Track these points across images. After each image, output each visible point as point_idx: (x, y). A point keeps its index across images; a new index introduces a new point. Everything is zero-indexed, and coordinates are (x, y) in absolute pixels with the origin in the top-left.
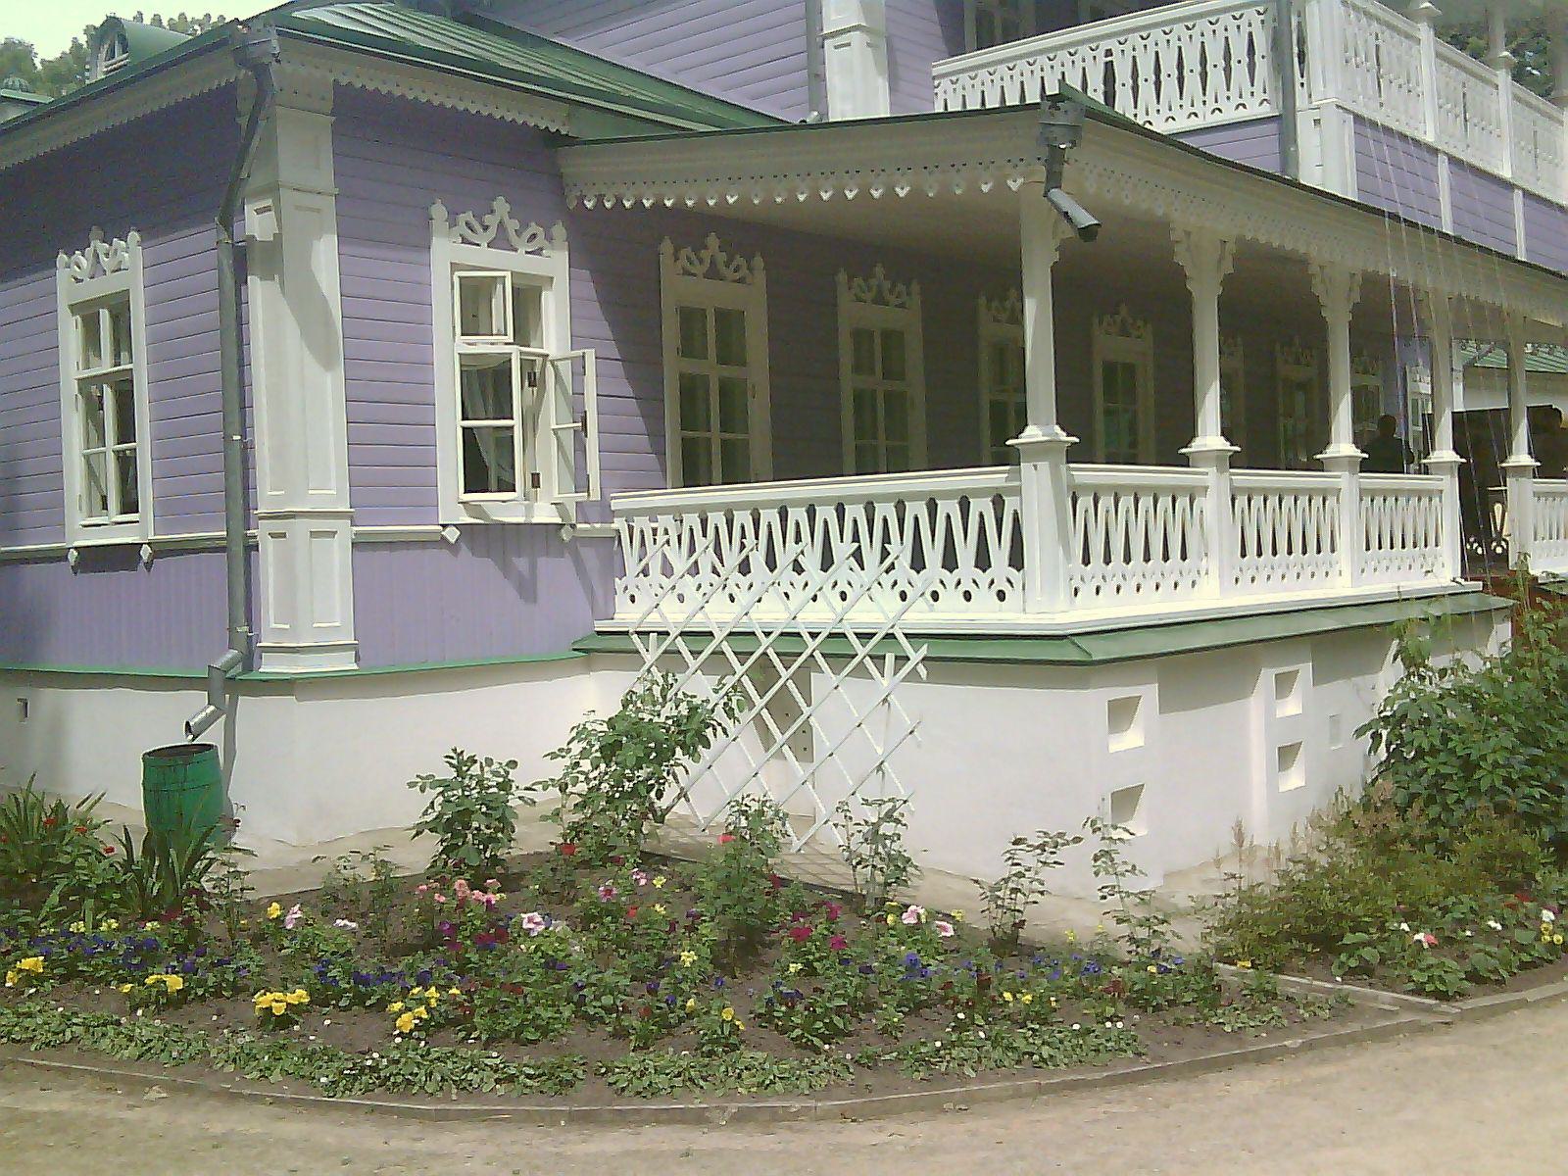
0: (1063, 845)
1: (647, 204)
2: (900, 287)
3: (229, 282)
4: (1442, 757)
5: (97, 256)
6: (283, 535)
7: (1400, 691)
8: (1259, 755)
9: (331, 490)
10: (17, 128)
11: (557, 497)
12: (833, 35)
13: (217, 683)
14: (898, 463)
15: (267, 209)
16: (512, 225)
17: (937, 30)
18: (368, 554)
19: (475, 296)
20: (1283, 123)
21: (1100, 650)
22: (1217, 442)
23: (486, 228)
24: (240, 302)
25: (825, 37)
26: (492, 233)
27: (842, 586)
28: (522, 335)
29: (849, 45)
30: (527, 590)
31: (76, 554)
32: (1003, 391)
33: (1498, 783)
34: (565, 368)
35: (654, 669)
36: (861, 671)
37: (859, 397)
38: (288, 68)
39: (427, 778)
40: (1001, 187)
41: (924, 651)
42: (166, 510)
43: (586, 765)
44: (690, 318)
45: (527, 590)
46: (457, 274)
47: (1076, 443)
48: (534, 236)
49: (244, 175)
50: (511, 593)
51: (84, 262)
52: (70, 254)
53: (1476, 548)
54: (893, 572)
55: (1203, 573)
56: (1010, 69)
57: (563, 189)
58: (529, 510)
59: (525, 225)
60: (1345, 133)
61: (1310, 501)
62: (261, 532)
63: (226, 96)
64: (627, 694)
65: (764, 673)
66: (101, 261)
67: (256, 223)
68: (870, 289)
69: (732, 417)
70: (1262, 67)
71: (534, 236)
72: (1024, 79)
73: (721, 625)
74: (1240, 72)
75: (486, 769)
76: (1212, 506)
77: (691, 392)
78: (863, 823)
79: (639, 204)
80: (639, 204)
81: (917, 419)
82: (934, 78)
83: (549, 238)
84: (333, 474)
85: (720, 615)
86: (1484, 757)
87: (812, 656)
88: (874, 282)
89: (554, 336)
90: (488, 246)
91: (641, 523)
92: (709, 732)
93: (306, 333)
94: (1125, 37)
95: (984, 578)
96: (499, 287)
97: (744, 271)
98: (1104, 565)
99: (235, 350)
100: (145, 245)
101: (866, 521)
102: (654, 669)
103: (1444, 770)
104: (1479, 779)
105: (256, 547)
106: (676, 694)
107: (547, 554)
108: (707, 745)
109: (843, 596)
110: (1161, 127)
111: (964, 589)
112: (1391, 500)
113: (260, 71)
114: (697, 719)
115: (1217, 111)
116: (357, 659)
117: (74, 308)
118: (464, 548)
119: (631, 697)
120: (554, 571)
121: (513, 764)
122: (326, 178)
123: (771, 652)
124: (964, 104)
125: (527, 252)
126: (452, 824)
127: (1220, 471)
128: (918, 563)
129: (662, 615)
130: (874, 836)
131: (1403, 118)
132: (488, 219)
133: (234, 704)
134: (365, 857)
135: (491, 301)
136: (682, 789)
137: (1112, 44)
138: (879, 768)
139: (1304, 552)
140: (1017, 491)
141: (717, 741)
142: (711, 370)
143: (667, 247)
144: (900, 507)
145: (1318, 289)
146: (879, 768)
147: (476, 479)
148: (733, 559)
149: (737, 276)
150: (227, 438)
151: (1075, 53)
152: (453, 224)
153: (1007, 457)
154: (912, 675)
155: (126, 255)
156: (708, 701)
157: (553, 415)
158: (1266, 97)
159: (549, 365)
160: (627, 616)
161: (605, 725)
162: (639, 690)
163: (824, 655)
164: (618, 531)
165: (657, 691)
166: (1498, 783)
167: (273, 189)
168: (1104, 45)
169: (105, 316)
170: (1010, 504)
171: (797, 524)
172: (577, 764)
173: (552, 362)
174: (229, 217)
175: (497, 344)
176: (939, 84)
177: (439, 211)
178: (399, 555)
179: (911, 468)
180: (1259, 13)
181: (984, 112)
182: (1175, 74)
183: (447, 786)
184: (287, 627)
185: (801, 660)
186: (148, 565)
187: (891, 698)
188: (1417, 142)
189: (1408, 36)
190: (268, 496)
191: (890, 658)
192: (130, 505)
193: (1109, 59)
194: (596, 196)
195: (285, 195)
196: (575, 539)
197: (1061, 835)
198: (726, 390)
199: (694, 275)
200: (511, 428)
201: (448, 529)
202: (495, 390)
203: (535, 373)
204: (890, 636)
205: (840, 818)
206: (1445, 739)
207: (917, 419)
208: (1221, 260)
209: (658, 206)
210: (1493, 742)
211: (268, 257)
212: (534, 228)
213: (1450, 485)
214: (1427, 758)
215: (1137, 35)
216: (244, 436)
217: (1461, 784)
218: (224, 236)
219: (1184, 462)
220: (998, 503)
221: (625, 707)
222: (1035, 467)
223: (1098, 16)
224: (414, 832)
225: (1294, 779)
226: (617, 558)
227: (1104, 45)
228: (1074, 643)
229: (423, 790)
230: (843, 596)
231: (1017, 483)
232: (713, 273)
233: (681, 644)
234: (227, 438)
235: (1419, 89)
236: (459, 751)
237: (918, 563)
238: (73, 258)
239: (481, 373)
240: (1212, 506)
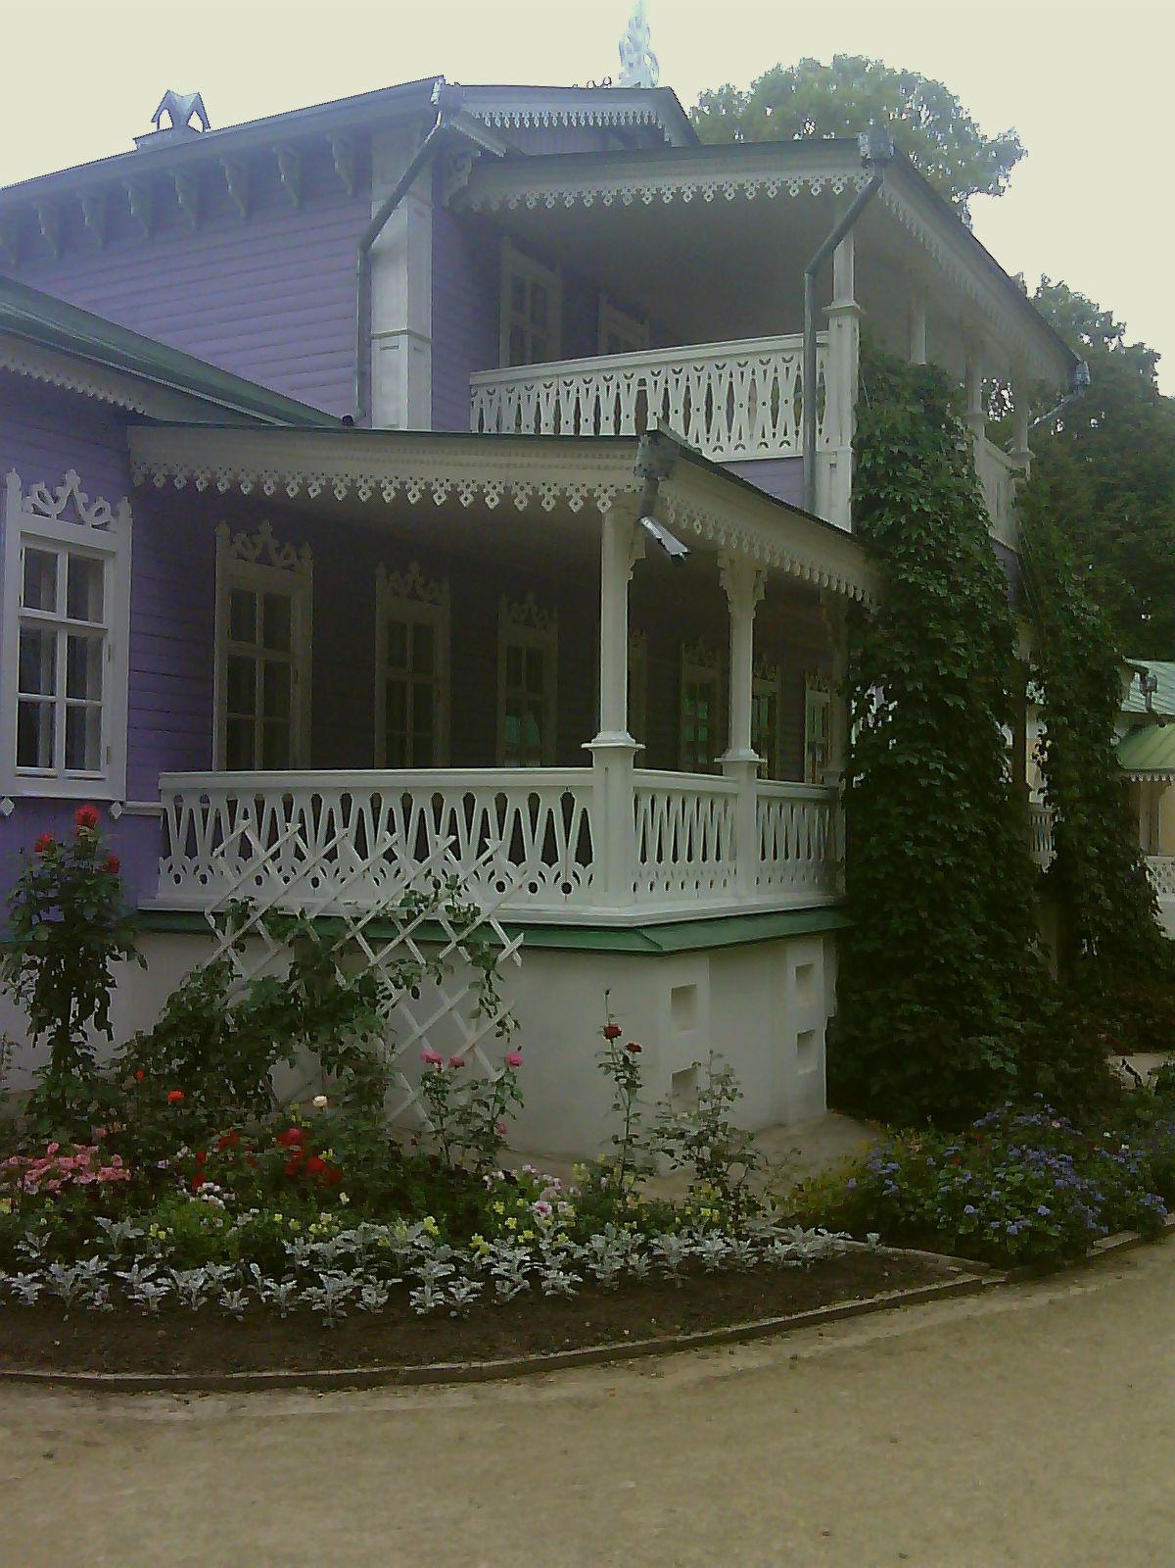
12: (381, 336)
16: (81, 498)
21: (668, 941)
22: (624, 739)
41: (520, 939)
47: (642, 749)
48: (100, 511)
61: (781, 809)
70: (786, 413)
71: (100, 511)
74: (764, 414)
83: (115, 514)
87: (403, 942)
95: (550, 872)
101: (528, 813)
123: (360, 939)
125: (93, 526)
128: (517, 855)
132: (60, 491)
139: (660, 860)
143: (223, 530)
145: (726, 582)
149: (99, 521)
179: (497, 765)
182: (704, 409)
185: (392, 945)
193: (643, 388)
198: (271, 671)
212: (101, 503)
219: (718, 770)
220: (567, 802)
227: (639, 375)
232: (264, 560)
237: (517, 855)
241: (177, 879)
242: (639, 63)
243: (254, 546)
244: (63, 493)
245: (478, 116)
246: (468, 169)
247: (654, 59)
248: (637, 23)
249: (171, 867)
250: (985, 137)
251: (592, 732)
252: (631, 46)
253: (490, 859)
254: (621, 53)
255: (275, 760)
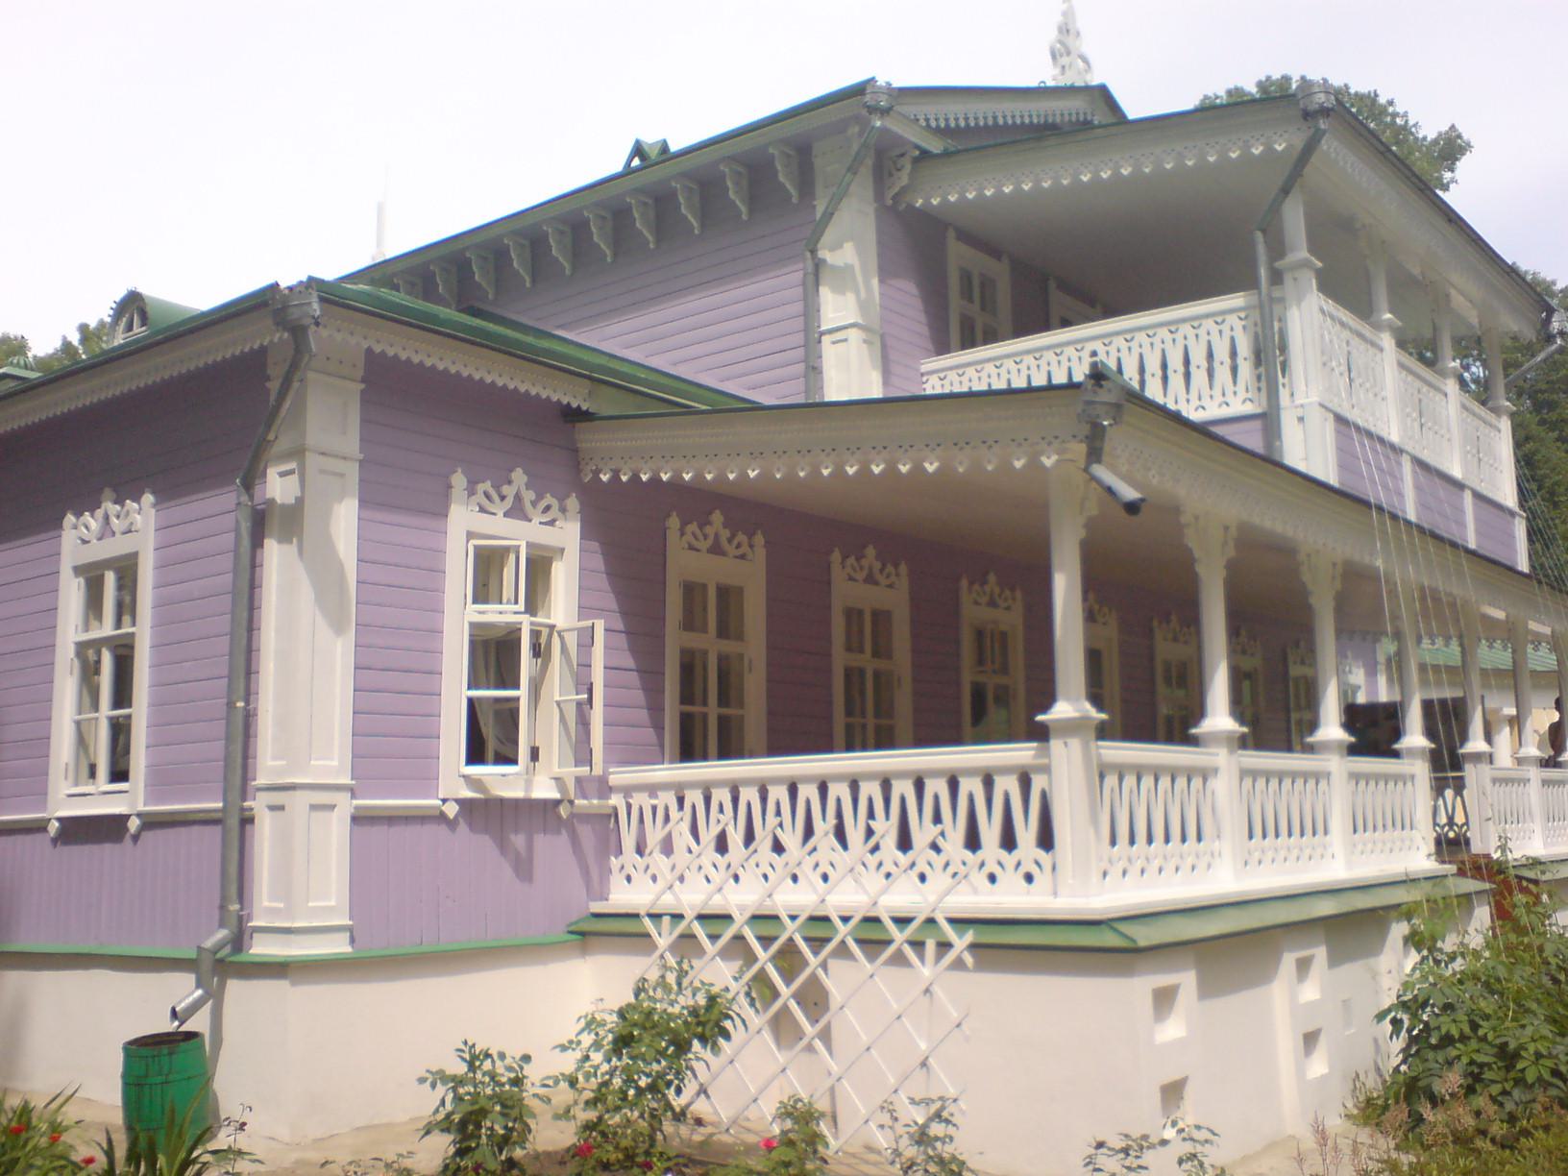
0: (1149, 1148)
1: (644, 478)
2: (890, 568)
3: (246, 542)
4: (1474, 1044)
5: (107, 518)
6: (282, 808)
7: (1418, 974)
8: (1286, 1042)
9: (332, 763)
10: (122, 356)
11: (557, 771)
13: (206, 965)
14: (885, 741)
15: (291, 472)
16: (529, 496)
17: (925, 331)
18: (378, 832)
19: (488, 565)
20: (1269, 420)
21: (1144, 935)
23: (503, 498)
24: (254, 565)
25: (822, 334)
26: (509, 503)
27: (825, 867)
28: (531, 608)
29: (846, 340)
30: (524, 868)
31: (57, 824)
32: (981, 672)
33: (1547, 1076)
34: (572, 640)
35: (668, 955)
36: (899, 959)
37: (848, 673)
38: (324, 333)
39: (437, 1072)
40: (1034, 463)
41: (969, 937)
42: (161, 781)
43: (597, 1057)
44: (692, 592)
45: (524, 868)
46: (474, 542)
48: (548, 508)
49: (271, 437)
50: (508, 871)
51: (94, 525)
52: (79, 514)
53: (1448, 832)
54: (815, 853)
55: (1216, 854)
56: (941, 379)
57: (579, 463)
58: (529, 785)
59: (540, 497)
60: (1326, 432)
62: (258, 804)
63: (254, 364)
64: (639, 981)
65: (789, 959)
66: (111, 522)
67: (278, 486)
68: (861, 568)
69: (728, 691)
70: (1245, 369)
71: (548, 508)
72: (1071, 364)
73: (742, 908)
74: (1223, 373)
75: (498, 1063)
76: (1223, 786)
77: (689, 668)
78: (912, 1124)
79: (635, 478)
80: (635, 478)
81: (904, 701)
82: (922, 375)
83: (563, 510)
84: (337, 742)
85: (741, 899)
86: (1522, 1047)
87: (843, 942)
88: (708, 530)
89: (562, 607)
90: (504, 516)
91: (639, 799)
92: (727, 1024)
93: (320, 599)
94: (1132, 335)
95: (1009, 859)
96: (512, 557)
97: (745, 549)
98: (1109, 847)
99: (245, 614)
100: (158, 507)
102: (668, 955)
103: (1481, 1058)
104: (1524, 1069)
105: (251, 820)
106: (692, 982)
107: (545, 832)
108: (727, 1036)
109: (825, 878)
110: (1195, 416)
111: (1025, 871)
112: (1181, 782)
113: (298, 332)
114: (716, 1011)
115: (1201, 409)
116: (352, 941)
117: (78, 570)
118: (463, 827)
119: (643, 985)
120: (550, 850)
121: (527, 1058)
122: (351, 443)
124: (1050, 379)
125: (541, 523)
126: (465, 1125)
127: (1231, 752)
128: (973, 842)
129: (725, 898)
130: (922, 1138)
131: (1371, 419)
132: (506, 489)
133: (222, 986)
134: (388, 1166)
135: (502, 570)
136: (701, 1085)
137: (1097, 346)
138: (924, 1064)
140: (1046, 769)
141: (738, 1034)
142: (709, 643)
143: (674, 522)
144: (854, 787)
146: (924, 1064)
147: (476, 753)
148: (708, 836)
149: (740, 552)
150: (231, 705)
151: (1061, 353)
152: (471, 492)
153: (1040, 734)
154: (958, 964)
155: (138, 517)
156: (727, 989)
157: (558, 688)
158: (1249, 395)
159: (555, 634)
160: (624, 896)
161: (615, 1015)
162: (653, 976)
163: (807, 939)
164: (615, 809)
165: (671, 978)
166: (1547, 1076)
167: (298, 453)
168: (1090, 347)
169: (110, 579)
170: (1038, 783)
171: (749, 805)
172: (587, 1058)
173: (559, 633)
174: (251, 479)
175: (506, 612)
176: (927, 380)
177: (459, 480)
178: (397, 831)
180: (1241, 319)
181: (1030, 390)
183: (458, 1081)
184: (282, 905)
186: (136, 838)
187: (936, 989)
188: (1381, 440)
189: (1373, 344)
190: (268, 766)
191: (931, 946)
192: (119, 774)
194: (611, 470)
195: (312, 460)
196: (572, 815)
197: (1145, 1137)
199: (698, 550)
200: (517, 699)
201: (447, 804)
202: (498, 659)
203: (540, 645)
204: (931, 921)
205: (886, 1118)
206: (1475, 1026)
207: (904, 701)
208: (1225, 543)
209: (655, 480)
210: (1529, 1030)
211: (290, 521)
212: (549, 499)
213: (1421, 770)
214: (1457, 1045)
215: (955, 371)
216: (247, 702)
217: (1502, 1073)
218: (244, 498)
221: (637, 996)
222: (1066, 744)
223: (1066, 323)
224: (422, 1133)
225: (1318, 1066)
226: (613, 838)
227: (1090, 347)
228: (1116, 930)
229: (433, 1086)
230: (825, 878)
231: (1045, 761)
232: (716, 549)
233: (698, 929)
234: (231, 705)
235: (1384, 393)
236: (470, 1043)
238: (82, 518)
239: (486, 643)
240: (1223, 786)
241: (629, 879)
242: (1070, 66)
243: (706, 537)
244: (509, 491)
245: (912, 117)
246: (908, 167)
247: (1085, 60)
248: (1065, 30)
249: (622, 867)
250: (1425, 138)
251: (1047, 700)
252: (1063, 50)
253: (815, 849)
254: (1054, 57)
255: (728, 750)
